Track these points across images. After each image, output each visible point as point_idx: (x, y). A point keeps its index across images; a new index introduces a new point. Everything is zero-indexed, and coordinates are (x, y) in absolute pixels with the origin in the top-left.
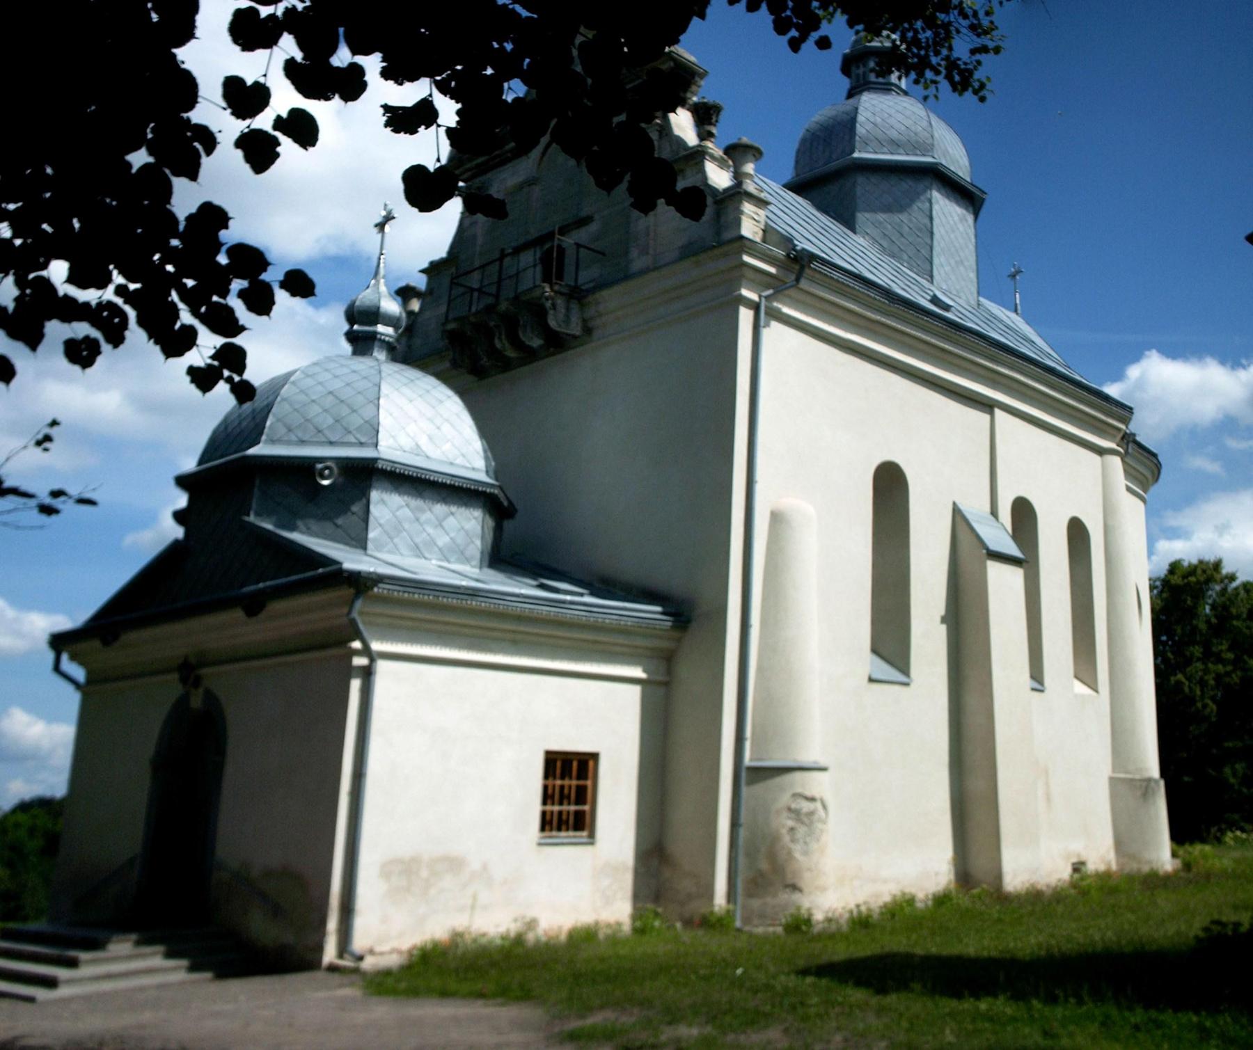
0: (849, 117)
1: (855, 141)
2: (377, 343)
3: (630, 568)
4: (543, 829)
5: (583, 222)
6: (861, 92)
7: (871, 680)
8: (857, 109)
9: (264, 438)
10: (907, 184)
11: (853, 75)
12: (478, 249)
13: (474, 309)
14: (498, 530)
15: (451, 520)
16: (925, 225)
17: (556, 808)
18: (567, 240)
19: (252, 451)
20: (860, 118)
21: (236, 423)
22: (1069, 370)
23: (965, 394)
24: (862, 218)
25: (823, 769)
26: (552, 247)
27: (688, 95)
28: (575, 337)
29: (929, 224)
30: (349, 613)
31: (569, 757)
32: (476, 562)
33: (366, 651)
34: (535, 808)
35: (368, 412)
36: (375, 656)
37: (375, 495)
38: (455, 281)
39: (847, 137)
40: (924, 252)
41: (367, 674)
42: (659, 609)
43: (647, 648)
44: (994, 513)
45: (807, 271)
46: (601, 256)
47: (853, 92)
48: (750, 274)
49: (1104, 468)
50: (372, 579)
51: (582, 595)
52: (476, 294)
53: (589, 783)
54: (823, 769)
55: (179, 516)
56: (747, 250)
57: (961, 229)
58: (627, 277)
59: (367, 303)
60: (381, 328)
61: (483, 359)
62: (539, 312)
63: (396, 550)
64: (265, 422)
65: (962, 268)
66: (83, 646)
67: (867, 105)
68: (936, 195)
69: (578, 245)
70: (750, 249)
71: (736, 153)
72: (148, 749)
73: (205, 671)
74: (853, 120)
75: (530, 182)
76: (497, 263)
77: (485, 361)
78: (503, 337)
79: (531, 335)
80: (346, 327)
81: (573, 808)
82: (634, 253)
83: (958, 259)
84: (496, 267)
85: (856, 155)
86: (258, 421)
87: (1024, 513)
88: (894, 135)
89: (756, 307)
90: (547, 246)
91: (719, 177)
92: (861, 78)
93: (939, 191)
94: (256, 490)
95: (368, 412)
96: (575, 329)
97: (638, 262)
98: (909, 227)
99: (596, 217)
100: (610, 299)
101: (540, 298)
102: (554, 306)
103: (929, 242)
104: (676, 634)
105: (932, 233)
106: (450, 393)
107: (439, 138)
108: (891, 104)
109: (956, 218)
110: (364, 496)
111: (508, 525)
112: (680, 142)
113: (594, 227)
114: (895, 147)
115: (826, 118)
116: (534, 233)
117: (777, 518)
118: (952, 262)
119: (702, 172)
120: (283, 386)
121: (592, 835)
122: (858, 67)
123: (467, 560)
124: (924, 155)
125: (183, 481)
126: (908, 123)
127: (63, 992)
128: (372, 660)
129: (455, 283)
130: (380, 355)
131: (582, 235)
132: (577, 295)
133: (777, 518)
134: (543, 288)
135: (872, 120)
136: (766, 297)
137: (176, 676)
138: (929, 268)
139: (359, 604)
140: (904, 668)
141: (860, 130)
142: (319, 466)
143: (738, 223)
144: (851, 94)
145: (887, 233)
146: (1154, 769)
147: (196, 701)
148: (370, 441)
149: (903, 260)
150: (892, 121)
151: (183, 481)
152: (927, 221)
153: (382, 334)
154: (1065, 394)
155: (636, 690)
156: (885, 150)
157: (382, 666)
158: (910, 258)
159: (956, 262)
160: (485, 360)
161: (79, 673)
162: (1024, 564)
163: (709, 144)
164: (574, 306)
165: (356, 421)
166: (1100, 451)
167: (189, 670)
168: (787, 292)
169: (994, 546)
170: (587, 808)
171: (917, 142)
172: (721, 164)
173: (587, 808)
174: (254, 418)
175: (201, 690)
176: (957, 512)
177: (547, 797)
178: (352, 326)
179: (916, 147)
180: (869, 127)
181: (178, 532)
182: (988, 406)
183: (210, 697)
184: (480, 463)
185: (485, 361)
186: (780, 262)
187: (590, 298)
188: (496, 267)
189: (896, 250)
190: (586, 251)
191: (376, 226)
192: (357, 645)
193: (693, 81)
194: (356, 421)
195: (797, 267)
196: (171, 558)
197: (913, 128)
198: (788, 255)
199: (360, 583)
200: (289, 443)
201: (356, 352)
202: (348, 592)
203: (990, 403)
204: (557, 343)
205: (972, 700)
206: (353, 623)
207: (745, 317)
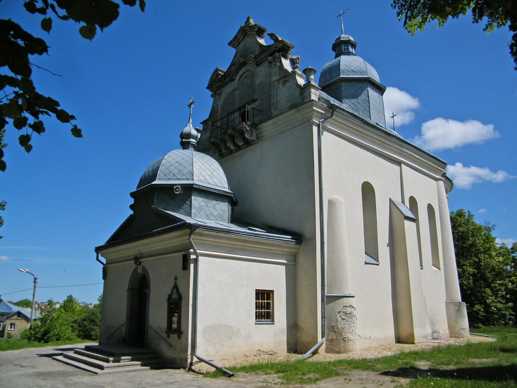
0: (337, 64)
1: (340, 72)
2: (190, 145)
3: (279, 223)
4: (256, 318)
5: (254, 101)
6: (340, 55)
7: (366, 263)
8: (340, 61)
9: (157, 178)
10: (359, 85)
11: (337, 51)
12: (219, 114)
13: (219, 134)
14: (233, 210)
15: (218, 206)
16: (366, 99)
17: (260, 311)
18: (249, 107)
19: (153, 183)
20: (341, 64)
21: (148, 174)
22: (241, 247)
23: (388, 157)
24: (344, 100)
25: (354, 297)
26: (245, 111)
27: (288, 55)
28: (254, 141)
29: (368, 99)
30: (189, 239)
31: (30, 345)
32: (227, 221)
33: (195, 253)
34: (253, 311)
35: (190, 168)
36: (199, 255)
37: (193, 197)
39: (337, 71)
40: (367, 109)
41: (196, 261)
42: (290, 237)
43: (289, 252)
44: (403, 202)
45: (335, 112)
46: (261, 112)
47: (337, 56)
48: (315, 114)
49: (438, 186)
50: (196, 226)
52: (219, 129)
54: (354, 297)
55: (132, 207)
56: (314, 105)
57: (378, 100)
58: (271, 118)
59: (187, 131)
60: (191, 140)
61: (223, 151)
62: (242, 133)
63: (201, 217)
64: (157, 173)
65: (379, 114)
66: (105, 251)
67: (343, 59)
68: (370, 89)
69: (254, 109)
70: (315, 104)
71: (307, 72)
72: (126, 286)
73: (141, 260)
74: (339, 65)
75: (235, 90)
76: (227, 117)
77: (224, 151)
78: (230, 142)
79: (239, 141)
80: (181, 140)
81: (266, 310)
82: (273, 110)
83: (378, 111)
84: (226, 118)
86: (155, 173)
87: (413, 201)
88: (353, 69)
89: (318, 126)
90: (242, 110)
91: (301, 81)
92: (340, 51)
93: (370, 88)
94: (155, 197)
95: (190, 168)
96: (254, 138)
97: (274, 112)
98: (361, 100)
99: (259, 99)
100: (267, 127)
101: (241, 127)
102: (38, 382)
103: (368, 105)
104: (297, 246)
105: (369, 102)
106: (215, 161)
108: (351, 59)
109: (376, 97)
110: (190, 197)
111: (235, 208)
112: (286, 71)
113: (258, 103)
114: (354, 73)
116: (237, 106)
117: (330, 202)
118: (376, 112)
119: (296, 79)
120: (162, 160)
121: (273, 321)
122: (338, 48)
123: (224, 220)
124: (364, 75)
125: (132, 195)
126: (358, 64)
128: (197, 256)
129: (213, 125)
130: (191, 149)
131: (254, 105)
132: (254, 126)
133: (331, 203)
134: (243, 124)
135: (346, 64)
136: (322, 122)
137: (133, 261)
138: (369, 114)
139: (192, 236)
140: (377, 259)
141: (341, 67)
143: (310, 96)
145: (353, 103)
146: (459, 299)
147: (140, 271)
148: (191, 178)
149: (360, 112)
150: (352, 64)
151: (132, 195)
152: (367, 98)
153: (192, 142)
154: (424, 158)
155: (283, 268)
156: (351, 74)
157: (201, 258)
158: (362, 111)
159: (377, 112)
160: (224, 151)
161: (104, 261)
162: (416, 221)
163: (297, 70)
164: (254, 130)
165: (185, 171)
166: (436, 180)
167: (137, 259)
168: (328, 120)
170: (271, 310)
171: (361, 71)
172: (301, 76)
173: (271, 310)
174: (153, 172)
175: (141, 267)
176: (391, 201)
177: (257, 307)
179: (361, 73)
180: (344, 66)
181: (132, 212)
182: (399, 163)
183: (144, 269)
184: (226, 186)
185: (224, 151)
186: (324, 108)
187: (259, 126)
188: (226, 118)
189: (357, 109)
191: (188, 106)
192: (192, 250)
193: (289, 50)
194: (185, 171)
195: (332, 111)
196: (131, 219)
197: (360, 66)
198: (328, 106)
199: (192, 228)
200: (165, 179)
202: (188, 231)
203: (400, 162)
204: (248, 143)
205: (400, 272)
206: (190, 242)
207: (315, 129)
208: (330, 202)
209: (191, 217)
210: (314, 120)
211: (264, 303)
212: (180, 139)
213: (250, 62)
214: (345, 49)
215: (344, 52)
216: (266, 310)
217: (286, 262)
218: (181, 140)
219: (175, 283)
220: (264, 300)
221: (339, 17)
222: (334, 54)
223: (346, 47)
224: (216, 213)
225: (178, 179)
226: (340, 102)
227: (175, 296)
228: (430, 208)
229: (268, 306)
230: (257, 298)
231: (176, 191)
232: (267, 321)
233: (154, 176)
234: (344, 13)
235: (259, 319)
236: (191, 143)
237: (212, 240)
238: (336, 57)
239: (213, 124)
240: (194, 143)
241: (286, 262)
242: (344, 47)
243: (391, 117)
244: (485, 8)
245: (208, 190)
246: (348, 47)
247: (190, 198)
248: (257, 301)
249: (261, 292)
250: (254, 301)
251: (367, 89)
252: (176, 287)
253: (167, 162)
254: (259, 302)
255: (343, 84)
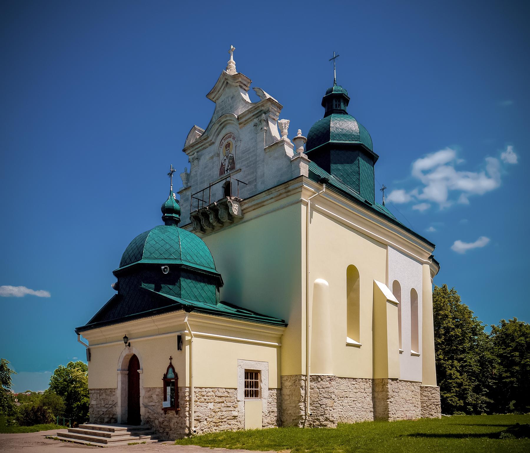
17: (249, 389)
24: (333, 166)
38: (193, 196)
41: (190, 342)
51: (251, 314)
53: (259, 380)
81: (254, 389)
85: (330, 141)
107: (348, 211)
112: (274, 138)
113: (241, 173)
115: (318, 126)
120: (146, 237)
125: (116, 274)
127: (109, 444)
138: (359, 188)
142: (163, 267)
144: (327, 114)
152: (357, 169)
156: (341, 139)
165: (172, 250)
166: (422, 263)
169: (388, 298)
170: (259, 389)
177: (246, 386)
178: (164, 214)
181: (117, 292)
182: (384, 245)
190: (240, 182)
191: (168, 174)
201: (166, 224)
208: (317, 286)
209: (181, 298)
210: (303, 199)
211: (248, 381)
212: (162, 213)
213: (232, 122)
214: (336, 105)
215: (335, 110)
216: (254, 389)
217: (277, 344)
218: (163, 214)
219: (171, 363)
220: (253, 379)
221: (332, 60)
222: (323, 110)
223: (338, 103)
224: (204, 295)
225: (166, 259)
226: (328, 173)
227: (171, 375)
228: (414, 294)
229: (256, 385)
230: (246, 377)
231: (164, 271)
232: (255, 399)
233: (140, 255)
234: (338, 56)
235: (248, 397)
236: (174, 218)
237: (201, 321)
238: (325, 116)
239: (192, 196)
240: (177, 219)
241: (277, 344)
242: (336, 103)
243: (381, 190)
244: (480, 405)
245: (194, 270)
246: (340, 103)
247: (179, 279)
248: (246, 380)
249: (250, 372)
250: (243, 380)
251: (358, 158)
252: (171, 366)
253: (152, 239)
254: (248, 381)
255: (332, 152)
